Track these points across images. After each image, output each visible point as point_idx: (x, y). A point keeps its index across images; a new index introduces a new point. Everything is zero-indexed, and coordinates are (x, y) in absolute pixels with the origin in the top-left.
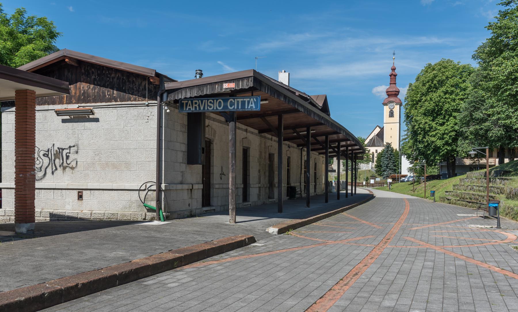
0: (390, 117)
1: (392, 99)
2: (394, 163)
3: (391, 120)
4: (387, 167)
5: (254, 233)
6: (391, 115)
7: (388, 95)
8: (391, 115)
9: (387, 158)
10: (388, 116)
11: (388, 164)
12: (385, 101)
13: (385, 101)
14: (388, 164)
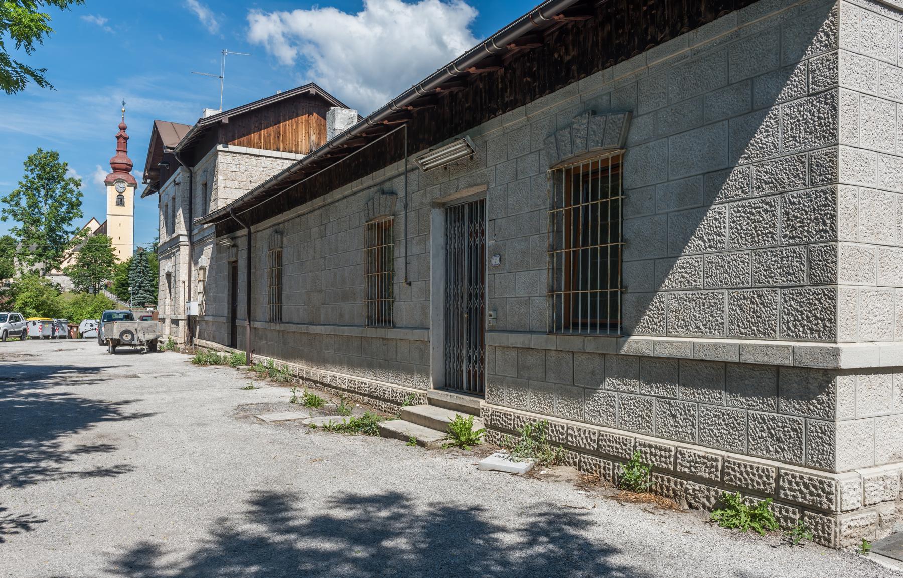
0: (118, 204)
1: (121, 176)
2: (150, 281)
3: (120, 210)
4: (140, 287)
5: (862, 558)
6: (121, 201)
7: (114, 169)
8: (121, 201)
9: (140, 272)
10: (115, 204)
11: (142, 282)
12: (109, 178)
13: (109, 178)
14: (142, 282)
